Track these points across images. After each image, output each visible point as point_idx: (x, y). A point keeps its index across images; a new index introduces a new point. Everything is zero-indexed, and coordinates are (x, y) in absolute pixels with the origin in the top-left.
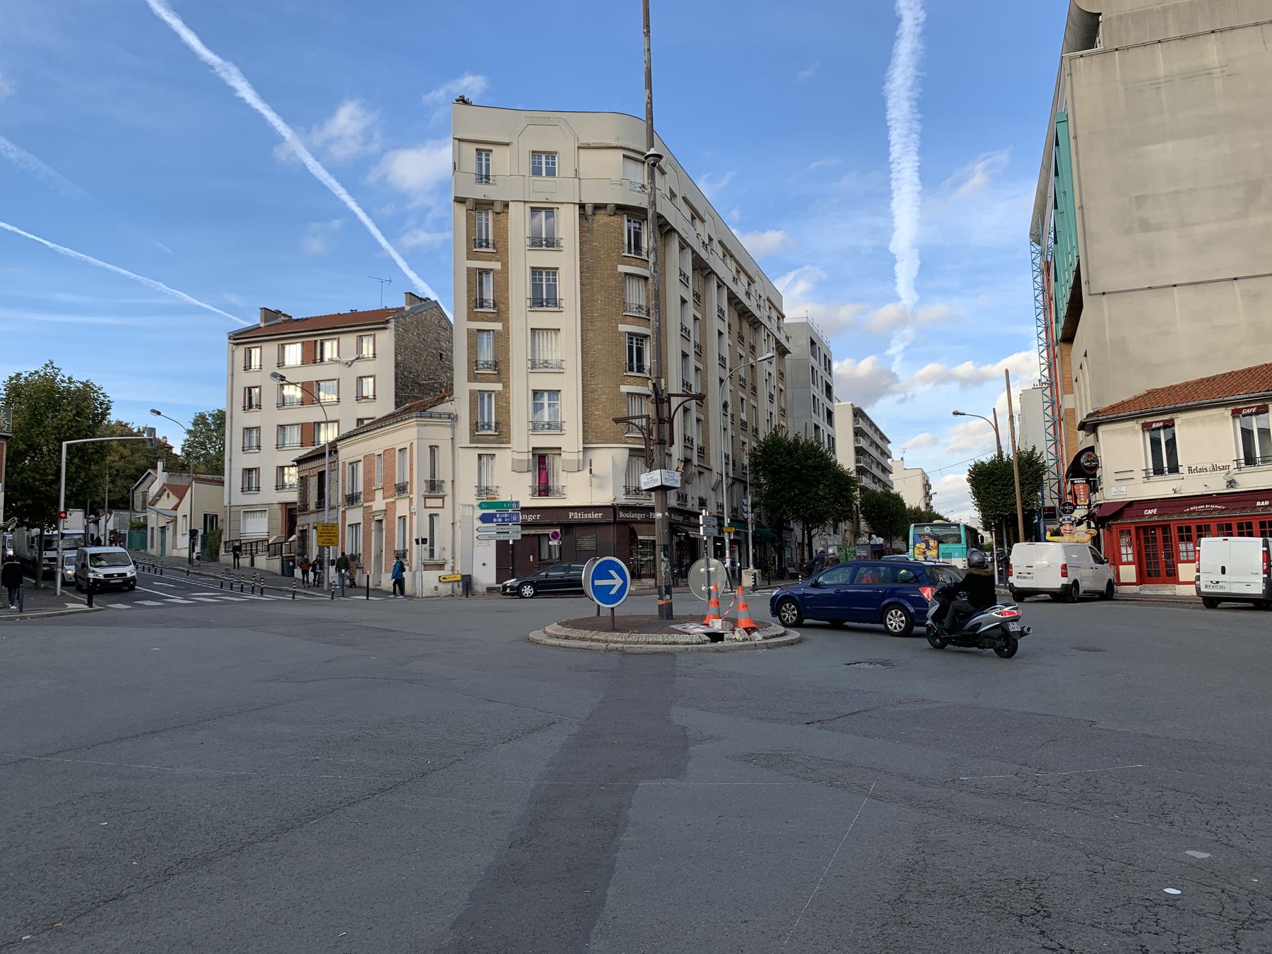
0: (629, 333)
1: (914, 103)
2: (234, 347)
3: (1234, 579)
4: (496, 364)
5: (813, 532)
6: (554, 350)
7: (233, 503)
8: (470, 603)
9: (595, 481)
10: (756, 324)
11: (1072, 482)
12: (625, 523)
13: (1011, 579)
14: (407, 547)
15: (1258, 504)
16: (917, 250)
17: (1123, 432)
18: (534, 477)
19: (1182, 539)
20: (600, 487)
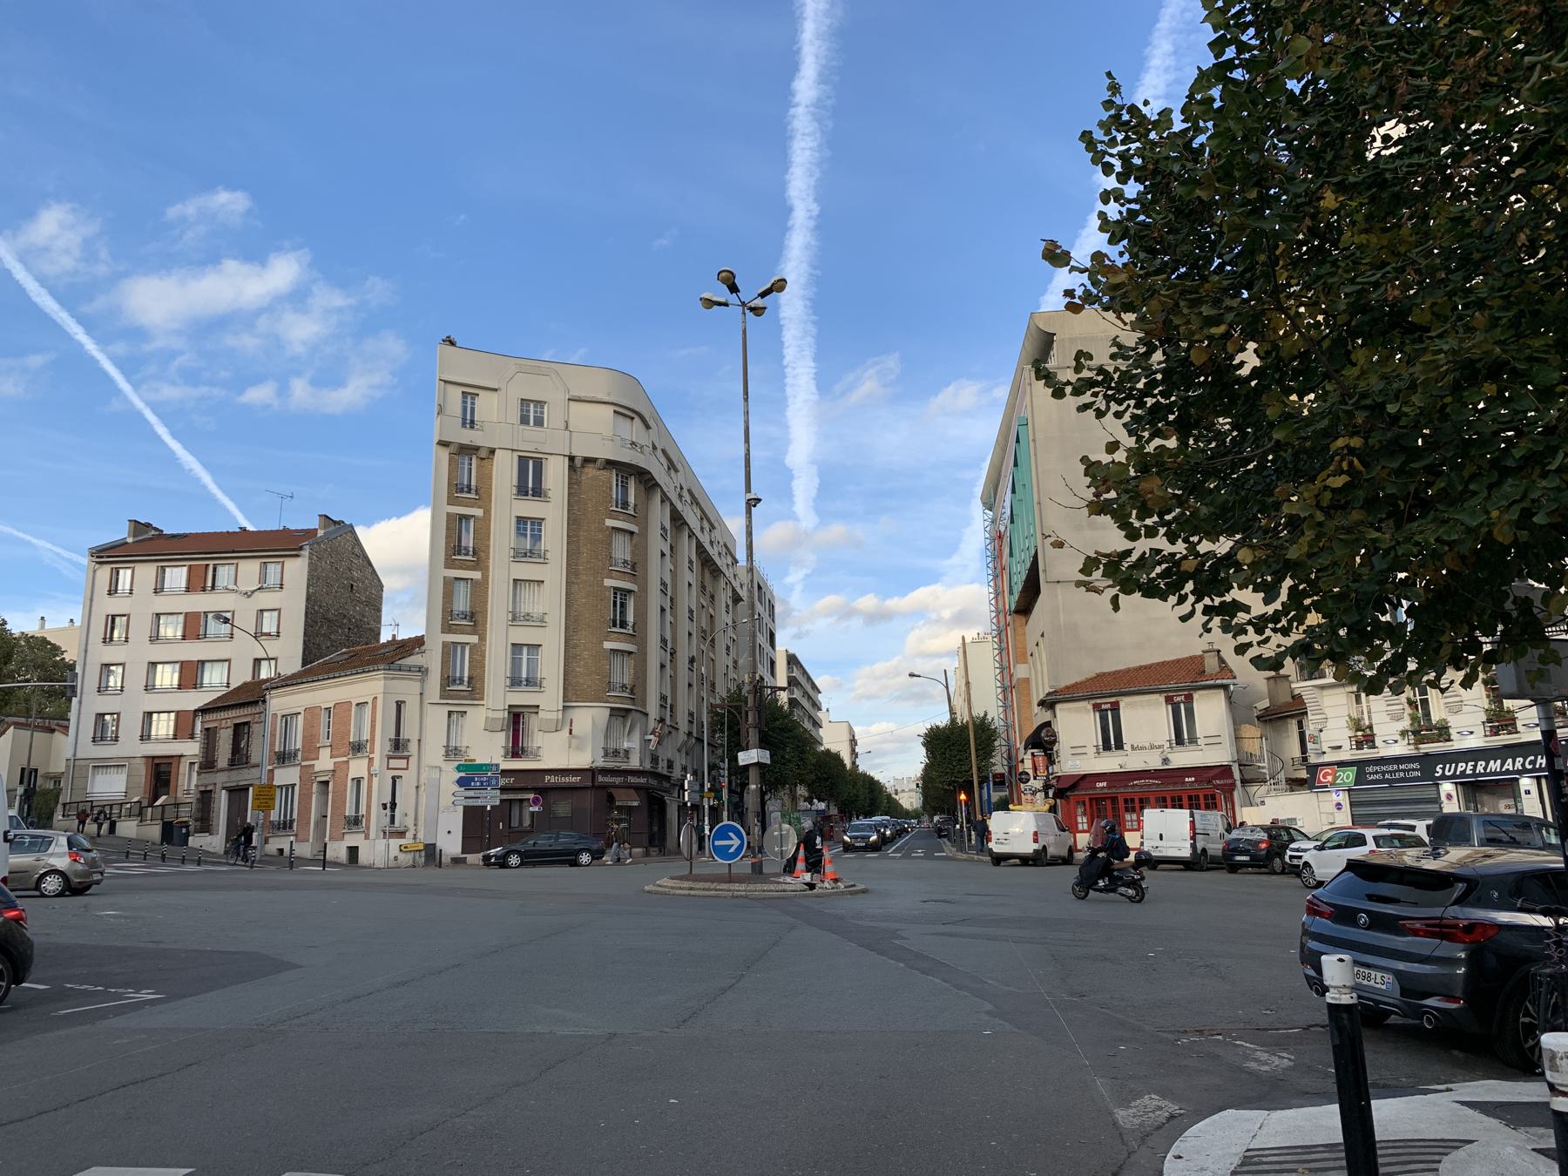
0: (615, 588)
1: (808, 303)
2: (97, 566)
3: (1169, 844)
4: (473, 615)
5: (767, 797)
6: (534, 603)
7: (79, 756)
8: (433, 871)
9: (574, 742)
10: (716, 572)
11: (1033, 754)
12: (604, 787)
13: (991, 845)
14: (363, 811)
15: (1187, 780)
16: (815, 468)
17: (1078, 710)
18: (507, 738)
19: (1127, 810)
20: (580, 748)
